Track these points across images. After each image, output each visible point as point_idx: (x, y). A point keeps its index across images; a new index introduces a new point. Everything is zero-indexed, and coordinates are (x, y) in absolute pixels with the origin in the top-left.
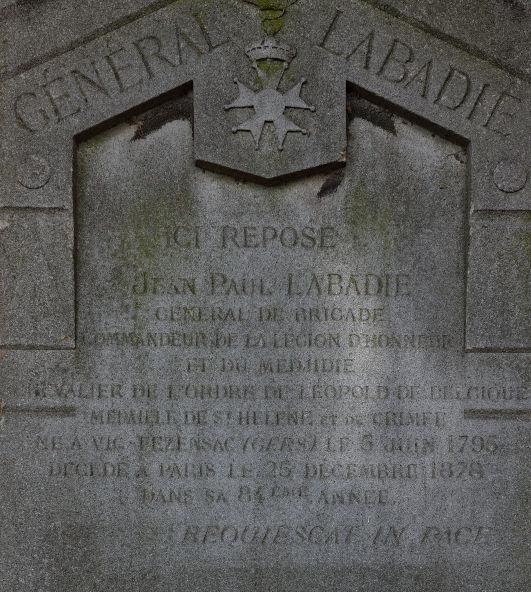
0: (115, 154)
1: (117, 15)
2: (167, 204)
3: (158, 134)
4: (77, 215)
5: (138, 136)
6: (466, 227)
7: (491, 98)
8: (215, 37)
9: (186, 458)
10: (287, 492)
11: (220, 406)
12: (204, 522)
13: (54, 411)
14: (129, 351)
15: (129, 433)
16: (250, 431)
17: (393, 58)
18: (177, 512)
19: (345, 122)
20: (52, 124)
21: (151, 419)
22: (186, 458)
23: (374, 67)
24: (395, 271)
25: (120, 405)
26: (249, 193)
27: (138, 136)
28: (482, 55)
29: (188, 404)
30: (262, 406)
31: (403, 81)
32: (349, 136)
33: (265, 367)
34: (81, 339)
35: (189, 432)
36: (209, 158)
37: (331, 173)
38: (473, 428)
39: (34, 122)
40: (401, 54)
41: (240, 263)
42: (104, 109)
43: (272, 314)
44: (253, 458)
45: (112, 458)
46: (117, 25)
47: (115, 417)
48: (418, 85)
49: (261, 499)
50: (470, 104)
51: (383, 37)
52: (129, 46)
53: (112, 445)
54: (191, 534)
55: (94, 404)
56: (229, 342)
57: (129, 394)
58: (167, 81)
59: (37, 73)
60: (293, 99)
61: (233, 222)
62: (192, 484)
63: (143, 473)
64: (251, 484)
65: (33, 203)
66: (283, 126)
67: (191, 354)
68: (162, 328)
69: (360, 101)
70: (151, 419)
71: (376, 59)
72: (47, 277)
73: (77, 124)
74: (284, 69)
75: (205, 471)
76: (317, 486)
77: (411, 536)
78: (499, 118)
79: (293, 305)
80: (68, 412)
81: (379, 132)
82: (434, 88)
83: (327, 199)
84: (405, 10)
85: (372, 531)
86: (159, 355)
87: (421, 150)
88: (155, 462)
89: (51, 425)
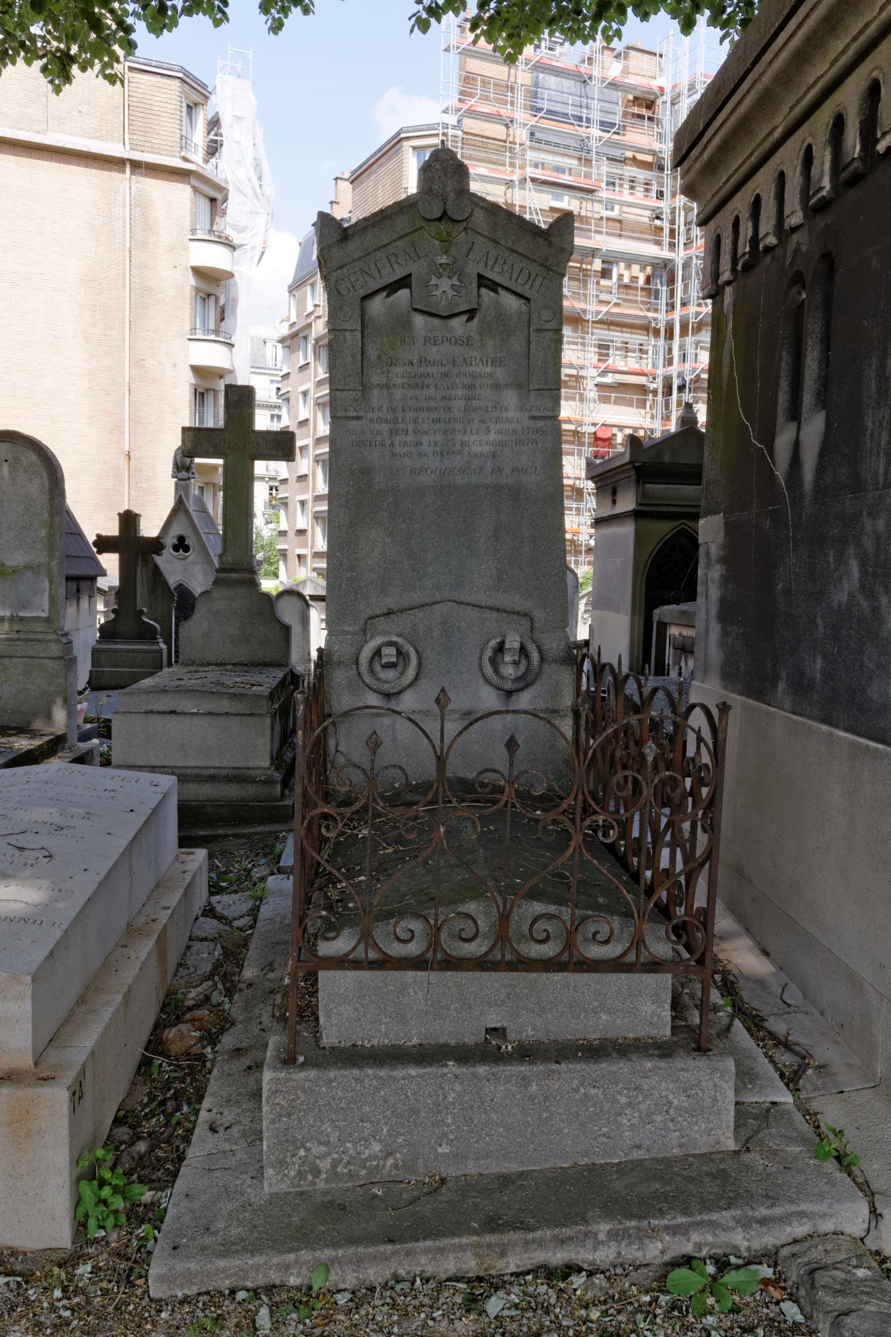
0: (377, 305)
1: (379, 245)
2: (400, 325)
3: (396, 295)
4: (362, 332)
5: (388, 296)
6: (529, 336)
7: (539, 280)
8: (420, 254)
9: (410, 438)
10: (454, 453)
11: (424, 415)
12: (418, 466)
13: (353, 418)
14: (385, 391)
15: (386, 428)
16: (438, 426)
17: (761, 1143)
18: (407, 461)
19: (848, 1179)
20: (352, 293)
21: (395, 421)
22: (410, 438)
23: (489, 267)
24: (498, 355)
25: (381, 415)
26: (436, 321)
27: (388, 296)
28: (535, 261)
29: (411, 415)
30: (443, 415)
31: (502, 272)
32: (479, 296)
33: (444, 398)
34: (365, 387)
35: (411, 427)
36: (419, 307)
37: (471, 313)
38: (532, 424)
39: (344, 292)
40: (501, 261)
41: (432, 352)
42: (373, 286)
43: (446, 375)
44: (439, 438)
45: (379, 438)
46: (379, 249)
47: (380, 420)
48: (508, 275)
49: (442, 455)
50: (530, 283)
51: (493, 253)
52: (384, 258)
53: (379, 433)
54: (413, 471)
55: (370, 415)
56: (428, 387)
57: (385, 410)
58: (400, 273)
59: (345, 270)
60: (455, 281)
61: (429, 334)
62: (413, 449)
63: (392, 445)
64: (438, 449)
65: (344, 327)
66: (451, 293)
67: (412, 393)
68: (399, 381)
69: (483, 281)
70: (395, 421)
71: (490, 263)
72: (350, 359)
73: (362, 292)
74: (453, 269)
75: (418, 444)
76: (466, 449)
77: (508, 471)
78: (543, 289)
79: (455, 371)
80: (359, 418)
81: (492, 294)
82: (515, 276)
83: (469, 324)
84: (502, 242)
85: (490, 469)
86: (398, 393)
87: (510, 302)
88: (397, 440)
89: (353, 424)
